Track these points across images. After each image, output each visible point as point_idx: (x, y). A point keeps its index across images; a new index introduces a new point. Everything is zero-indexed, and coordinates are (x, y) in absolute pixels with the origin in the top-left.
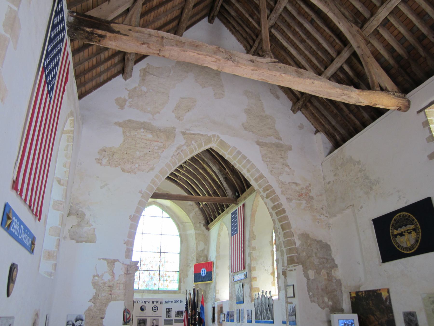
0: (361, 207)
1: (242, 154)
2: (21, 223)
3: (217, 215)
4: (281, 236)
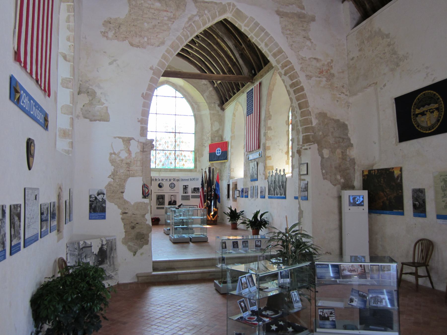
0: (385, 85)
1: (260, 26)
2: (31, 98)
3: (232, 95)
4: (298, 115)
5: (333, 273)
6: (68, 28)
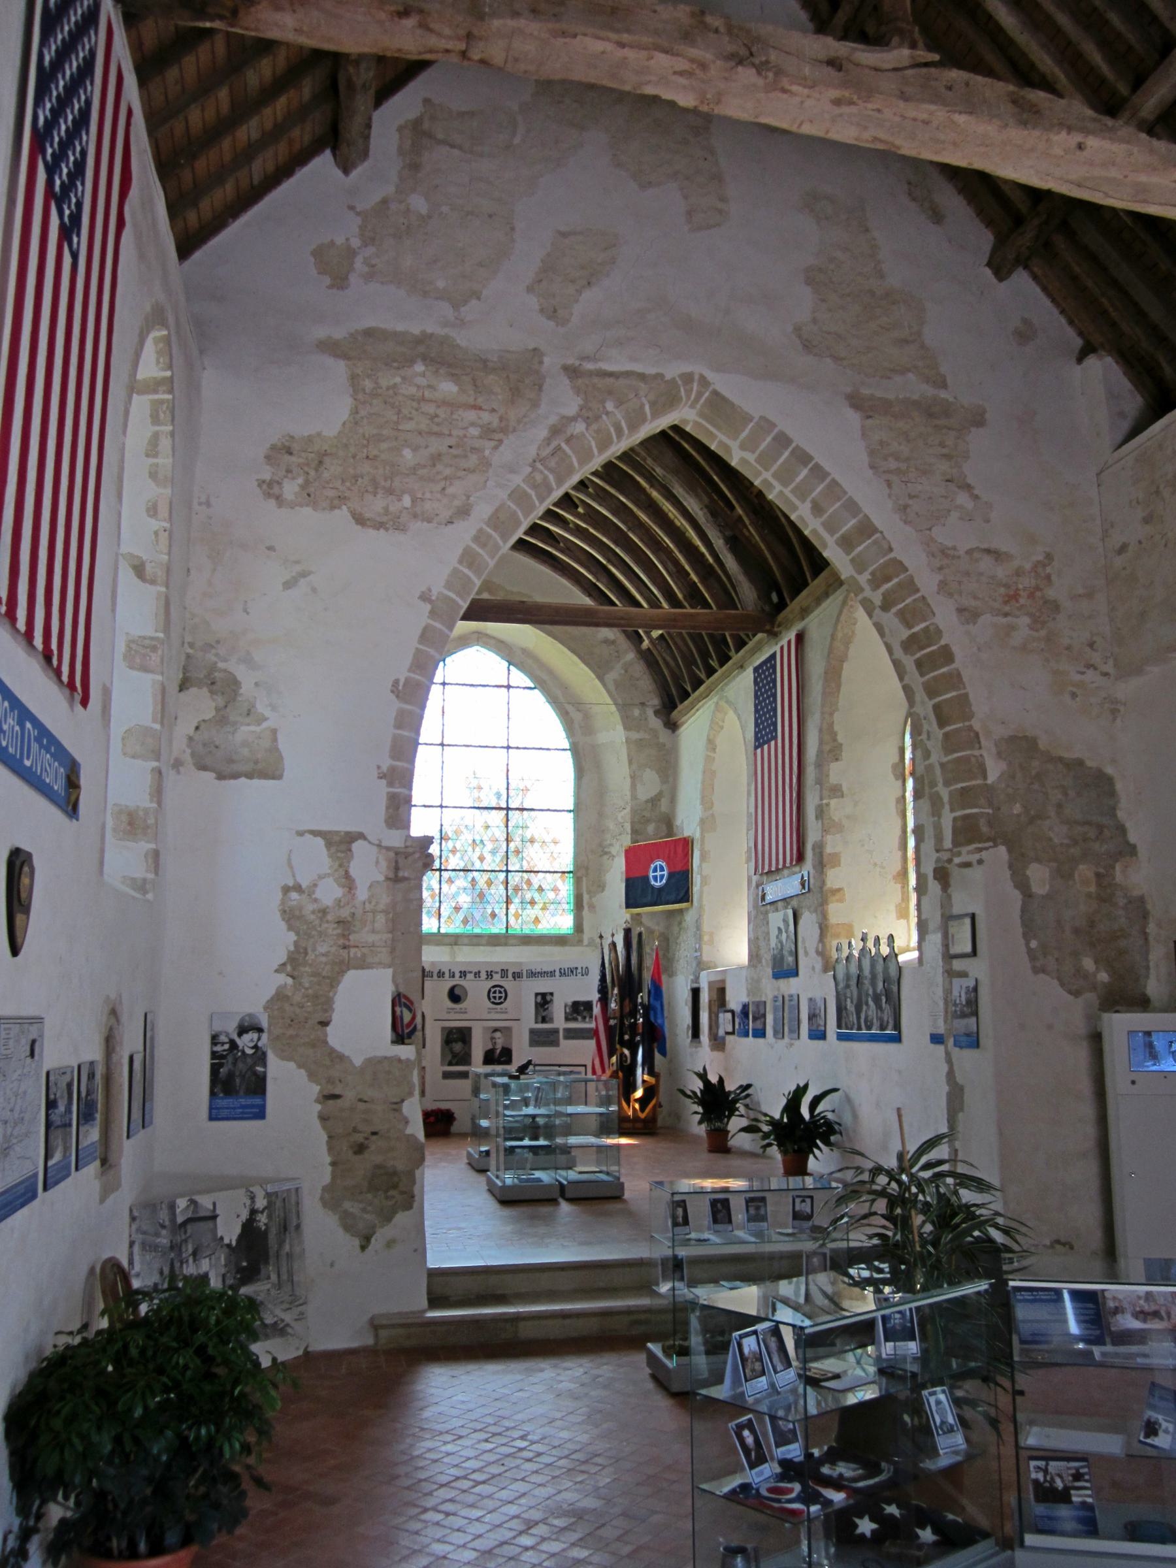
1: (794, 445)
3: (703, 676)
5: (1079, 1322)
6: (153, 475)
